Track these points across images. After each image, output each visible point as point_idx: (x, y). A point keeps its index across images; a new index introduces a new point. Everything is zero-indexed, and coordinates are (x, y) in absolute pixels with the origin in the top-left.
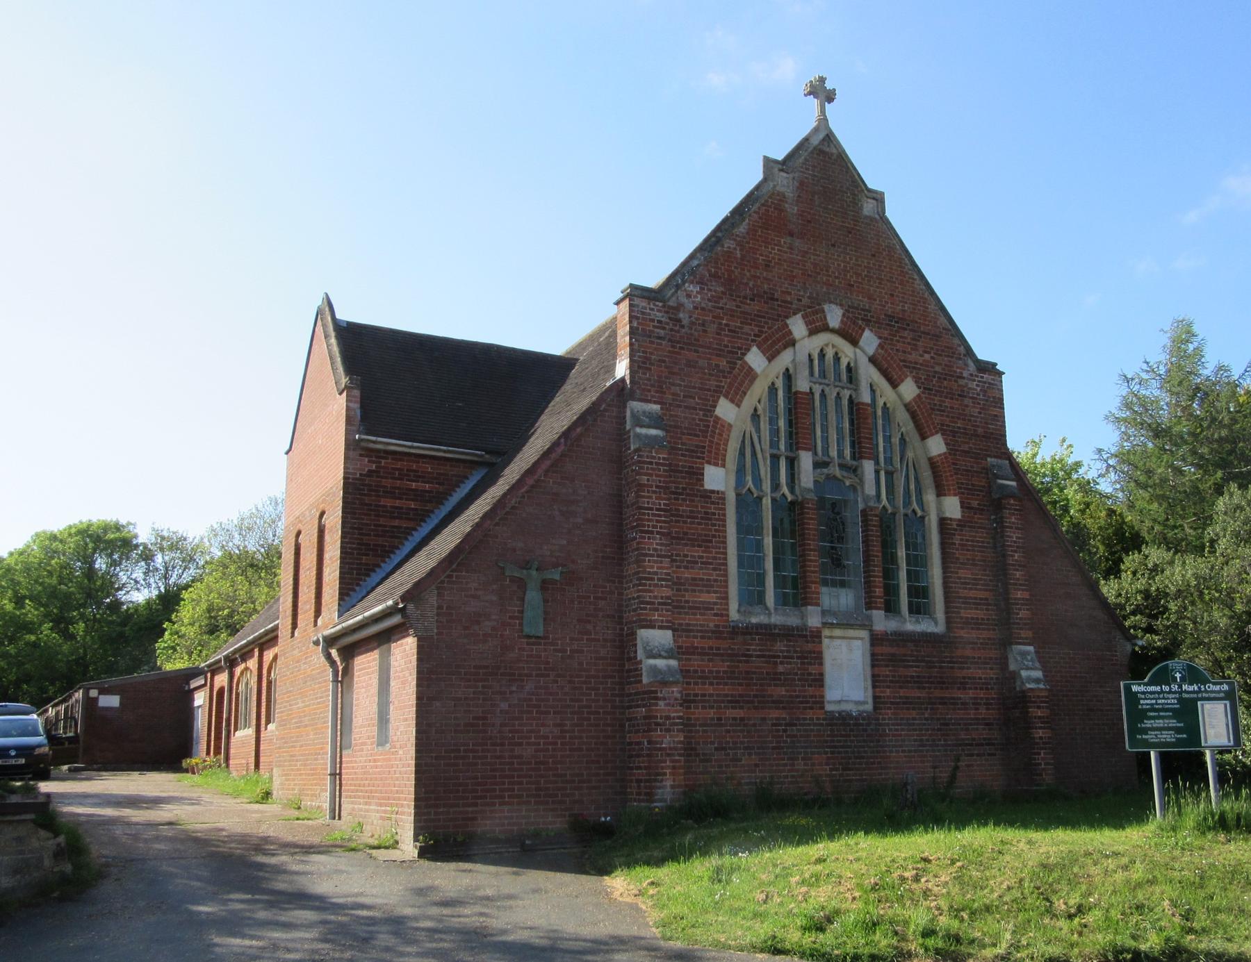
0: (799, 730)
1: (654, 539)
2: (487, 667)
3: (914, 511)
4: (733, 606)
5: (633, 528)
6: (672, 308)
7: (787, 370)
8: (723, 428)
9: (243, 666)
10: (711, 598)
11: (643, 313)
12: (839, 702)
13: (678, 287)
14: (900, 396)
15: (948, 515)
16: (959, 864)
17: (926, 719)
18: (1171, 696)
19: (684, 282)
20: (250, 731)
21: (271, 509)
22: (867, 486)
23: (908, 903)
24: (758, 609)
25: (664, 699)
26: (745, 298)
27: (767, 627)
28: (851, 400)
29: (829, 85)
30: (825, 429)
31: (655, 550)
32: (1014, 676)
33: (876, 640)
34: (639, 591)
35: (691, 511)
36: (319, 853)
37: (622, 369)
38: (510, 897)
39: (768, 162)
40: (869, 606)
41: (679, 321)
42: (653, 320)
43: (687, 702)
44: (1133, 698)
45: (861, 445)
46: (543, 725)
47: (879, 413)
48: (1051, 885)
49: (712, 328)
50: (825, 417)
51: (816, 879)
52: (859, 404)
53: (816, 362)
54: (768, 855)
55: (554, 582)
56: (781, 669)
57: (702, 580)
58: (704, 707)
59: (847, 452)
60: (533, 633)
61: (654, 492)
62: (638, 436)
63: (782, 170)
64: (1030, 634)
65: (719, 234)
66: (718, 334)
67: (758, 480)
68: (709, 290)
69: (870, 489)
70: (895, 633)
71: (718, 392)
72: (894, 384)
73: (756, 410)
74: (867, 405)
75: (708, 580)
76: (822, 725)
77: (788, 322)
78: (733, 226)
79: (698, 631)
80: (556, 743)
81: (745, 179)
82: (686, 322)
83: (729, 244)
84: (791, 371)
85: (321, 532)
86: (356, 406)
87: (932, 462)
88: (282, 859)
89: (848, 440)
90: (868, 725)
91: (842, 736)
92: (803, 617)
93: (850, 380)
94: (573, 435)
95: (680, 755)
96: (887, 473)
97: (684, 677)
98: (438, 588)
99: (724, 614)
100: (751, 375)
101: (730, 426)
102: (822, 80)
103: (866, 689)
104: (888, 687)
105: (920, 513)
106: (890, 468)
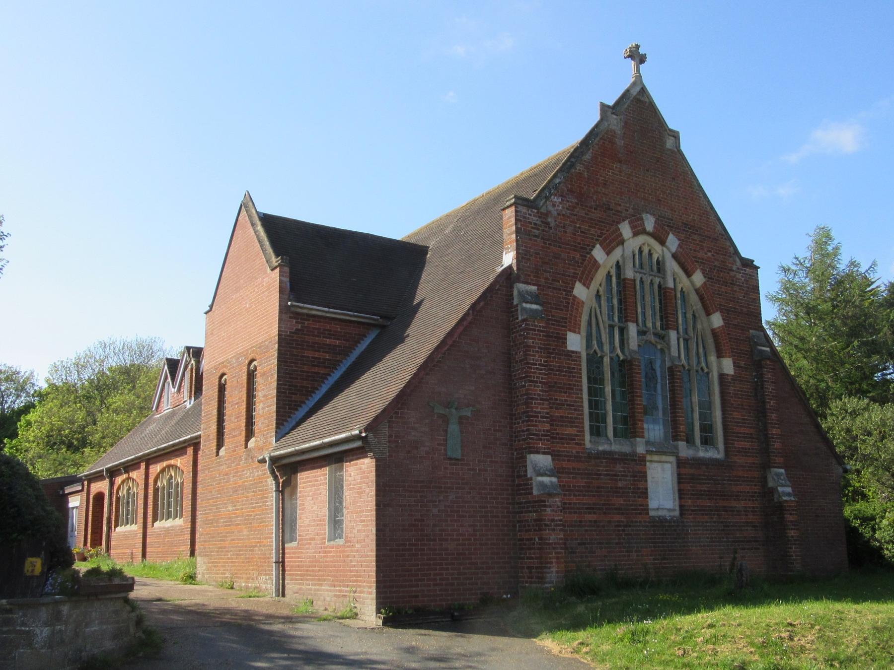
0: (632, 530)
1: (538, 387)
2: (422, 482)
3: (702, 369)
4: (587, 437)
5: (521, 378)
7: (618, 262)
8: (577, 304)
9: (125, 476)
10: (572, 431)
11: (525, 217)
12: (658, 509)
13: (547, 198)
15: (726, 371)
16: (817, 627)
17: (715, 522)
19: (551, 194)
20: (135, 528)
21: (101, 351)
22: (672, 349)
23: (792, 655)
24: (602, 439)
25: (550, 506)
26: (591, 207)
27: (611, 453)
28: (660, 286)
29: (641, 51)
30: (644, 307)
31: (539, 395)
32: (772, 491)
33: (681, 463)
34: (529, 425)
35: (559, 367)
36: (300, 622)
37: (509, 258)
38: (480, 654)
39: (604, 107)
40: (676, 438)
41: (548, 224)
42: (531, 223)
43: (565, 508)
45: (667, 319)
46: (462, 526)
47: (679, 295)
48: (887, 642)
49: (570, 230)
50: (643, 297)
51: (714, 640)
52: (666, 288)
53: (637, 256)
54: (665, 622)
55: (467, 418)
56: (620, 484)
57: (567, 417)
58: (570, 513)
59: (658, 324)
60: (454, 456)
61: (537, 352)
62: (524, 309)
63: (613, 113)
64: (781, 460)
65: (573, 160)
66: (574, 234)
67: (600, 344)
68: (567, 201)
69: (674, 353)
70: (694, 459)
71: (575, 278)
72: (689, 274)
73: (598, 291)
74: (671, 289)
75: (571, 418)
76: (647, 526)
77: (620, 226)
78: (582, 153)
79: (566, 456)
80: (470, 540)
81: (587, 120)
82: (552, 225)
83: (579, 167)
84: (621, 263)
85: (251, 376)
86: (286, 280)
87: (714, 332)
88: (277, 627)
89: (658, 314)
90: (678, 526)
91: (660, 534)
92: (633, 445)
93: (659, 270)
94: (478, 308)
95: (561, 548)
96: (684, 339)
97: (563, 491)
98: (389, 422)
99: (581, 444)
100: (595, 265)
101: (583, 303)
102: (637, 47)
103: (674, 500)
104: (690, 498)
105: (706, 370)
106: (686, 336)
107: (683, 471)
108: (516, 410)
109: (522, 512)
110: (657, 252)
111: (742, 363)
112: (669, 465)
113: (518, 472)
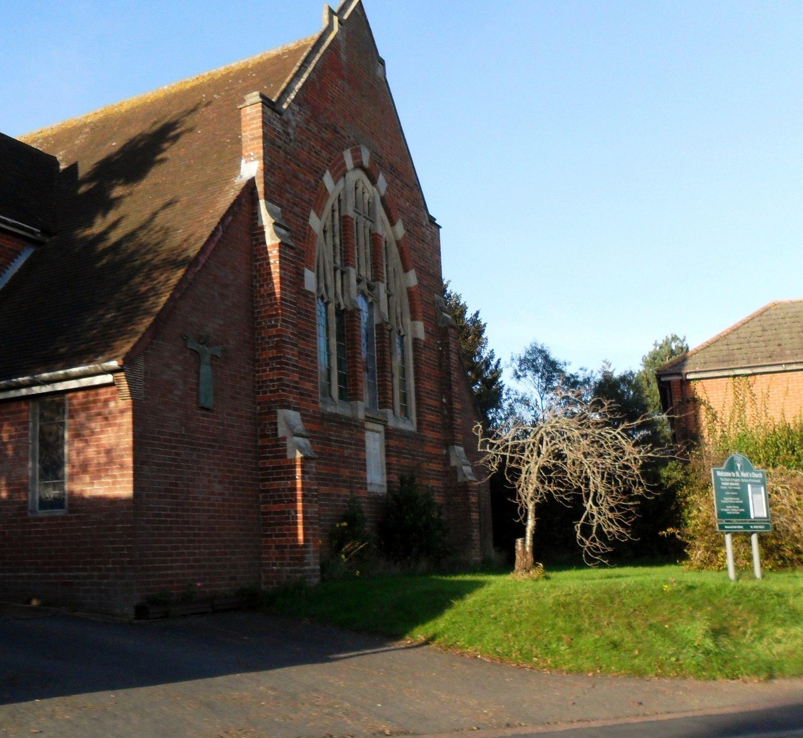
6: (284, 121)
14: (394, 233)
18: (736, 480)
32: (455, 470)
37: (251, 168)
41: (288, 134)
44: (717, 478)
84: (342, 197)
87: (410, 292)
107: (393, 443)
108: (261, 355)
109: (268, 480)
110: (369, 192)
111: (430, 329)
112: (377, 435)
113: (262, 430)
